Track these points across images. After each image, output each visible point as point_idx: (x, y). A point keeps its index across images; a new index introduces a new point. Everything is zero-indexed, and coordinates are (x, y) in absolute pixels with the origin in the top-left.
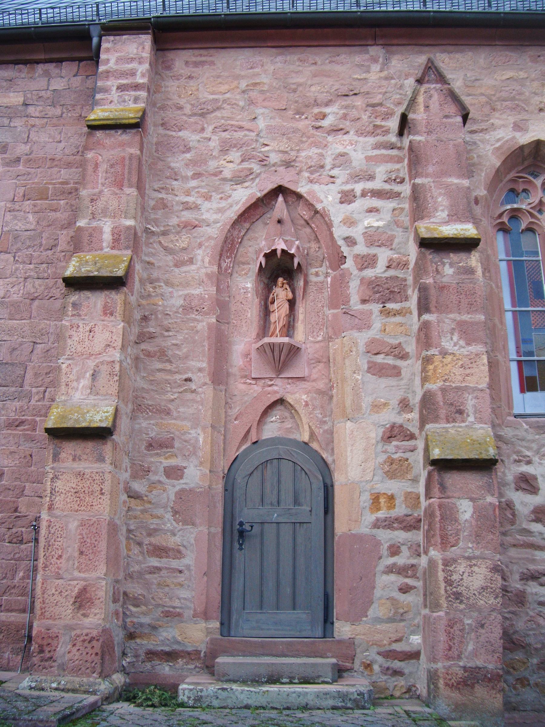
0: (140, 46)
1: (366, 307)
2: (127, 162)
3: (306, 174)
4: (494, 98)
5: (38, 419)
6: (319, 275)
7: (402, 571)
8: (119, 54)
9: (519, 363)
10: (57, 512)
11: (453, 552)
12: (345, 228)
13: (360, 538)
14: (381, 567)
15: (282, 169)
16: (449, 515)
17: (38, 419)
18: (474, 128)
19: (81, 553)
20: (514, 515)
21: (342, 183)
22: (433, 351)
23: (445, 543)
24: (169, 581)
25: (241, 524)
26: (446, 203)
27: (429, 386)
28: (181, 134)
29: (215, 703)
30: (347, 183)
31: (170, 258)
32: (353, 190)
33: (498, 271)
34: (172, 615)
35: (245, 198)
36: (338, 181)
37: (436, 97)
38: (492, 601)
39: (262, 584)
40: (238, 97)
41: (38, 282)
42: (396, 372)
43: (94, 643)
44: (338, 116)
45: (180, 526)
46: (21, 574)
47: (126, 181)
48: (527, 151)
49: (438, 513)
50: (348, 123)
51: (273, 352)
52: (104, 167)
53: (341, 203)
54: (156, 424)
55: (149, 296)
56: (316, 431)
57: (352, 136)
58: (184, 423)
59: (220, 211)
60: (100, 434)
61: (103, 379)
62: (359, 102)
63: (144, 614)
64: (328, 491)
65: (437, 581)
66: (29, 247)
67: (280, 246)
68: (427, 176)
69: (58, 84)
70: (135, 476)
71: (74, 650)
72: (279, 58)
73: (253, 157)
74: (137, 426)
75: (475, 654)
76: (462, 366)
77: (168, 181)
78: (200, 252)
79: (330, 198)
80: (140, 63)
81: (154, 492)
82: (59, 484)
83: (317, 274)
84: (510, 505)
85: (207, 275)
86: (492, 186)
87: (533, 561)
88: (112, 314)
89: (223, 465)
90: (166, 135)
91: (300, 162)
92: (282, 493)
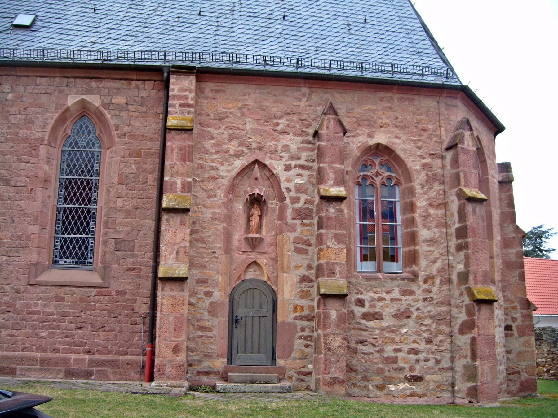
0: (189, 82)
1: (294, 221)
2: (187, 149)
3: (269, 155)
4: (360, 119)
5: (142, 267)
6: (273, 204)
7: (306, 338)
8: (179, 86)
9: (361, 248)
10: (164, 313)
11: (328, 331)
12: (286, 183)
13: (289, 324)
14: (297, 336)
15: (257, 151)
16: (327, 316)
17: (142, 267)
18: (349, 135)
19: (175, 330)
20: (354, 316)
21: (285, 161)
22: (323, 246)
23: (325, 328)
24: (206, 341)
25: (237, 317)
26: (333, 177)
27: (321, 262)
28: (209, 129)
29: (232, 391)
30: (288, 160)
31: (205, 193)
32: (290, 164)
33: (354, 205)
34: (208, 356)
35: (240, 165)
36: (284, 159)
37: (332, 122)
38: (342, 351)
39: (245, 343)
40: (237, 111)
41: (139, 200)
42: (306, 252)
43: (181, 367)
44: (285, 125)
45: (211, 317)
46: (137, 339)
47: (187, 158)
48: (372, 148)
49: (322, 315)
50: (289, 129)
51: (252, 240)
52: (176, 150)
53: (285, 170)
54: (200, 272)
55: (196, 212)
56: (270, 276)
57: (291, 136)
58: (212, 272)
59: (228, 171)
60: (182, 280)
61: (181, 254)
62: (295, 118)
63: (196, 355)
64: (275, 303)
65: (321, 342)
66: (134, 182)
67: (257, 191)
68: (325, 163)
69: (144, 94)
70: (191, 296)
71: (173, 370)
72: (257, 91)
73: (244, 144)
74: (191, 273)
75: (335, 372)
76: (335, 253)
77: (203, 154)
78: (219, 191)
79: (280, 168)
80: (190, 92)
81: (200, 303)
82: (164, 301)
83: (272, 204)
84: (352, 312)
85: (222, 203)
86: (354, 165)
87: (361, 336)
88: (184, 225)
89: (229, 291)
90: (202, 130)
91: (266, 148)
92: (255, 303)
